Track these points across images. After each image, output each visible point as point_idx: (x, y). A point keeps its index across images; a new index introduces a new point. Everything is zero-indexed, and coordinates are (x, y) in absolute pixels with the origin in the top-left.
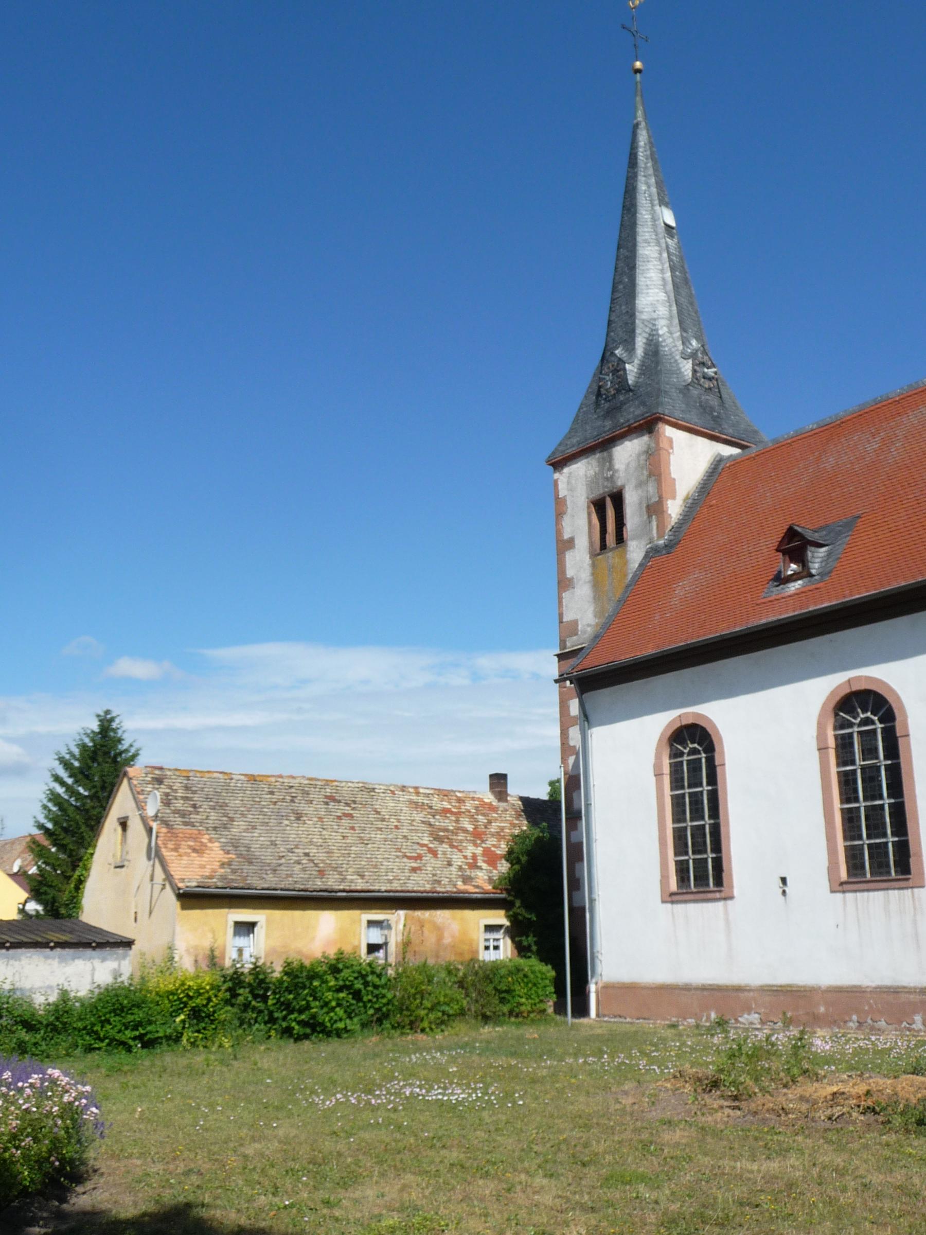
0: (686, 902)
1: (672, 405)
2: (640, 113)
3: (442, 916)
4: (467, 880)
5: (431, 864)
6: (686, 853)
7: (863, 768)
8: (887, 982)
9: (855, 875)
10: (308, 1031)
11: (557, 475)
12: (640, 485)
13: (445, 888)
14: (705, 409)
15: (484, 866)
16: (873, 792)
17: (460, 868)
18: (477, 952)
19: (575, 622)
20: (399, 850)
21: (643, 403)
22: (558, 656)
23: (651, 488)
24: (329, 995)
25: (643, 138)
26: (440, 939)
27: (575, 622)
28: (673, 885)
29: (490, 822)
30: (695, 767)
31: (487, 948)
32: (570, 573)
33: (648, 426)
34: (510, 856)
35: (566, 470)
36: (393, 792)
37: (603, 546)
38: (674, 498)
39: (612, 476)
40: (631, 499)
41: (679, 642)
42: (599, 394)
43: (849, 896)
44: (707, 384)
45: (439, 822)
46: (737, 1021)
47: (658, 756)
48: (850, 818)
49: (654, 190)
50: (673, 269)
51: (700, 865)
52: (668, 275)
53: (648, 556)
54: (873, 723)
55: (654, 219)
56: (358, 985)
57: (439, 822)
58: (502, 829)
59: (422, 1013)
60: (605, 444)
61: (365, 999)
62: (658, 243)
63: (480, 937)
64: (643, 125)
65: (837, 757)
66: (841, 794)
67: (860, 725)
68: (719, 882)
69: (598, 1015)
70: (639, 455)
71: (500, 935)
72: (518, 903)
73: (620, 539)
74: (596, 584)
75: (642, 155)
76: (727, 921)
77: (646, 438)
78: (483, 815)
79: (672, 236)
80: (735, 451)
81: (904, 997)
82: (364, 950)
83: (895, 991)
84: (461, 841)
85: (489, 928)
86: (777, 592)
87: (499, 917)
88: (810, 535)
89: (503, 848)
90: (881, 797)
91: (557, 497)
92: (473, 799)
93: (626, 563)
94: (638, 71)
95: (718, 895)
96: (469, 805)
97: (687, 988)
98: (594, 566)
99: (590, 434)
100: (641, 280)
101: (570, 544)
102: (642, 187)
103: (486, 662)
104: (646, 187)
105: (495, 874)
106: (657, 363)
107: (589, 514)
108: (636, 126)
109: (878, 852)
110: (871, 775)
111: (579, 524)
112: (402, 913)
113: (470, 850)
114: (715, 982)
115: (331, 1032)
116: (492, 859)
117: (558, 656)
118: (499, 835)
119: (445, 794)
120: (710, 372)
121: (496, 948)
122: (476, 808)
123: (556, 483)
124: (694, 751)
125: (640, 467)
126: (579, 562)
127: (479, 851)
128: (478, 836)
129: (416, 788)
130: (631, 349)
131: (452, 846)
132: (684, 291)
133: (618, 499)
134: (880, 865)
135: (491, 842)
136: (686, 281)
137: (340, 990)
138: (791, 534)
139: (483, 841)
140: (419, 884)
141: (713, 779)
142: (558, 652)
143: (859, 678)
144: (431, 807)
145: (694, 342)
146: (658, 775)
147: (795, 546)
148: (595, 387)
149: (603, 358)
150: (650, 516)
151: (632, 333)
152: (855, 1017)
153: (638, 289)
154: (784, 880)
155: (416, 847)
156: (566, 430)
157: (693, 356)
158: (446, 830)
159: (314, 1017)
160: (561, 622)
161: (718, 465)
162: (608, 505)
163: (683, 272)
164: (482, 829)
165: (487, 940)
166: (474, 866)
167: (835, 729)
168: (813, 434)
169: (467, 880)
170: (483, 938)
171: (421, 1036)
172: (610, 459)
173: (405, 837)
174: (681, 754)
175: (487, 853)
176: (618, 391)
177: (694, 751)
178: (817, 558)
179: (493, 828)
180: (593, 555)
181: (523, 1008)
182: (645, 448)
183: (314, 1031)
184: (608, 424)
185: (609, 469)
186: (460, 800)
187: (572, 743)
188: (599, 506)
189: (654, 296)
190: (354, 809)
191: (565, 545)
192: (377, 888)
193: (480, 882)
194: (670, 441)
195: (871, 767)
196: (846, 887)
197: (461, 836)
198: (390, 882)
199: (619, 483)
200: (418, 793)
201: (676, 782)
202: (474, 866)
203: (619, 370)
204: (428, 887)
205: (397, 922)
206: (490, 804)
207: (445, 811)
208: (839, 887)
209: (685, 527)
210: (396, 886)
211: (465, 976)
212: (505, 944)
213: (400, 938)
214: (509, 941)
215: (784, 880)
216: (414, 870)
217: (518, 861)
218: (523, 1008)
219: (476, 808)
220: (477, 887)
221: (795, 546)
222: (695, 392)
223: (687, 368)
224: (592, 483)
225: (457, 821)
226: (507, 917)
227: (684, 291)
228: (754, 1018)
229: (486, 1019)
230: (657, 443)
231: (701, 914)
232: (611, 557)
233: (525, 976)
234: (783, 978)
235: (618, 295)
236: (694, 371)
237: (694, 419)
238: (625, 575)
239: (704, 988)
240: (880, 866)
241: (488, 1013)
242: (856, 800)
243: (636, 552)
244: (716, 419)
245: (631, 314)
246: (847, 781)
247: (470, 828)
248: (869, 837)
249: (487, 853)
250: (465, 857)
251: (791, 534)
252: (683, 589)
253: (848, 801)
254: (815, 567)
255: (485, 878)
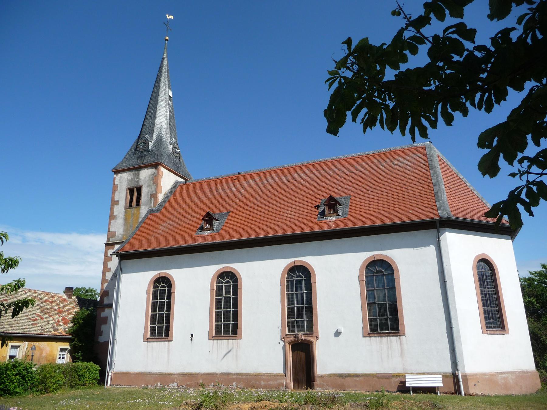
0: (153, 342)
1: (165, 160)
2: (165, 54)
3: (43, 345)
4: (55, 330)
5: (40, 322)
6: (155, 324)
7: (225, 298)
8: (225, 372)
9: (218, 334)
10: (2, 393)
11: (115, 176)
12: (149, 186)
13: (47, 333)
14: (174, 164)
15: (62, 324)
16: (227, 306)
17: (53, 325)
18: (56, 360)
19: (115, 232)
20: (27, 316)
21: (154, 157)
22: (106, 244)
23: (153, 188)
24: (14, 377)
25: (165, 63)
26: (41, 353)
27: (115, 232)
28: (149, 336)
29: (65, 306)
30: (163, 292)
31: (60, 358)
32: (115, 214)
33: (155, 166)
34: (74, 321)
35: (119, 175)
36: (25, 292)
37: (131, 205)
38: (161, 193)
39: (138, 181)
40: (145, 191)
41: (164, 246)
42: (136, 150)
43: (215, 341)
44: (176, 155)
45: (44, 305)
46: (168, 386)
47: (149, 287)
48: (218, 315)
49: (167, 83)
50: (170, 112)
51: (160, 328)
52: (168, 114)
53: (148, 212)
54: (230, 283)
55: (165, 93)
56: (25, 373)
57: (44, 305)
58: (70, 310)
59: (51, 385)
60: (137, 169)
61: (27, 379)
62: (166, 102)
63: (58, 353)
64: (166, 59)
65: (216, 293)
66: (216, 306)
67: (225, 283)
68: (167, 334)
69: (110, 385)
70: (150, 175)
71: (66, 353)
72: (76, 340)
73: (138, 204)
74: (126, 219)
75: (164, 69)
76: (169, 350)
77: (154, 170)
78: (62, 303)
79: (171, 101)
80: (183, 181)
81: (230, 377)
82: (8, 358)
83: (228, 374)
84: (53, 314)
85: (62, 350)
86: (200, 233)
87: (66, 346)
88: (215, 217)
89: (71, 317)
90: (230, 308)
91: (114, 184)
92: (58, 297)
93: (139, 213)
94: (167, 40)
95: (166, 340)
96: (56, 299)
97: (150, 374)
98: (126, 212)
99: (132, 162)
100: (158, 113)
101: (117, 202)
102: (163, 80)
103: (30, 235)
104: (164, 81)
105: (67, 328)
106: (161, 144)
107: (127, 193)
108: (164, 58)
109: (226, 327)
110: (227, 300)
111: (122, 196)
112: (27, 343)
113: (57, 317)
114: (364, 372)
115: (12, 393)
116: (65, 322)
117: (106, 244)
118: (69, 312)
119: (47, 294)
120: (178, 151)
121: (63, 358)
122: (59, 300)
123: (114, 179)
124: (163, 287)
125: (150, 180)
126: (120, 210)
127: (60, 318)
128: (60, 312)
129: (35, 290)
130: (152, 137)
131: (49, 316)
132: (172, 121)
133: (139, 189)
134: (227, 331)
135: (65, 315)
136: (173, 117)
137: (16, 375)
138: (208, 214)
139: (62, 314)
140: (36, 331)
141: (169, 297)
142: (106, 242)
143: (227, 267)
144: (41, 299)
145: (174, 139)
146: (148, 294)
147: (209, 219)
148: (135, 147)
149: (139, 137)
150: (151, 198)
151: (153, 131)
152: (212, 384)
153: (157, 116)
154: (192, 335)
155: (35, 315)
156: (121, 160)
157: (173, 144)
158: (47, 309)
159: (6, 387)
160: (109, 231)
161: (177, 183)
162: (135, 192)
163: (173, 114)
164: (61, 309)
165: (60, 355)
166: (58, 324)
167: (217, 283)
168: (212, 181)
169: (55, 330)
170: (58, 354)
171: (50, 394)
172: (138, 174)
173: (30, 311)
174: (158, 287)
175: (63, 319)
176: (144, 150)
177: (163, 287)
178: (216, 224)
179: (66, 309)
180: (126, 208)
181: (87, 382)
182: (153, 173)
183: (5, 393)
184: (139, 161)
185: (137, 178)
186: (53, 297)
187: (107, 278)
188: (131, 191)
189: (162, 119)
190: (8, 297)
191: (115, 203)
192: (18, 332)
193: (61, 331)
194: (163, 172)
195: (228, 297)
196: (214, 338)
197: (53, 312)
198: (23, 329)
199: (141, 184)
200: (35, 293)
201: (155, 297)
202: (58, 324)
203: (146, 143)
204: (39, 332)
205: (24, 347)
206: (65, 299)
207: (47, 301)
208: (212, 338)
209: (164, 204)
210: (26, 331)
211: (66, 369)
212: (67, 356)
213: (24, 353)
214: (69, 355)
215: (192, 335)
216: (34, 325)
217: (78, 323)
218: (87, 382)
219: (59, 300)
220: (59, 333)
221: (209, 219)
222: (172, 157)
223: (171, 147)
224: (130, 182)
225: (51, 305)
226: (70, 345)
227: (172, 121)
228: (175, 385)
229: (72, 387)
230: (158, 172)
231: (159, 346)
232: (133, 210)
233: (89, 369)
234: (187, 370)
235: (148, 116)
236: (173, 149)
237: (171, 167)
238: (138, 218)
239: (157, 374)
240: (227, 331)
241: (73, 385)
242: (221, 308)
243: (144, 210)
244: (178, 168)
245: (153, 124)
246: (218, 302)
247: (57, 308)
248: (224, 321)
249: (63, 319)
250: (55, 320)
251: (208, 214)
252: (163, 227)
253: (218, 309)
254: (215, 227)
255: (62, 330)
